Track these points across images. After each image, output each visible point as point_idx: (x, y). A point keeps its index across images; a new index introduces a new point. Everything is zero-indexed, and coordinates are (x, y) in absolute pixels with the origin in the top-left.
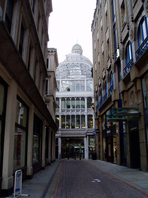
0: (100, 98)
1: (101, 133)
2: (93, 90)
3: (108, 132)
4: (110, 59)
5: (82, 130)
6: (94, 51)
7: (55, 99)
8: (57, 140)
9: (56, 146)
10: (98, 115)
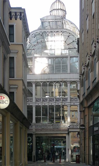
0: (86, 82)
1: (87, 129)
2: (78, 71)
3: (96, 129)
6: (82, 11)
7: (26, 84)
9: (29, 146)
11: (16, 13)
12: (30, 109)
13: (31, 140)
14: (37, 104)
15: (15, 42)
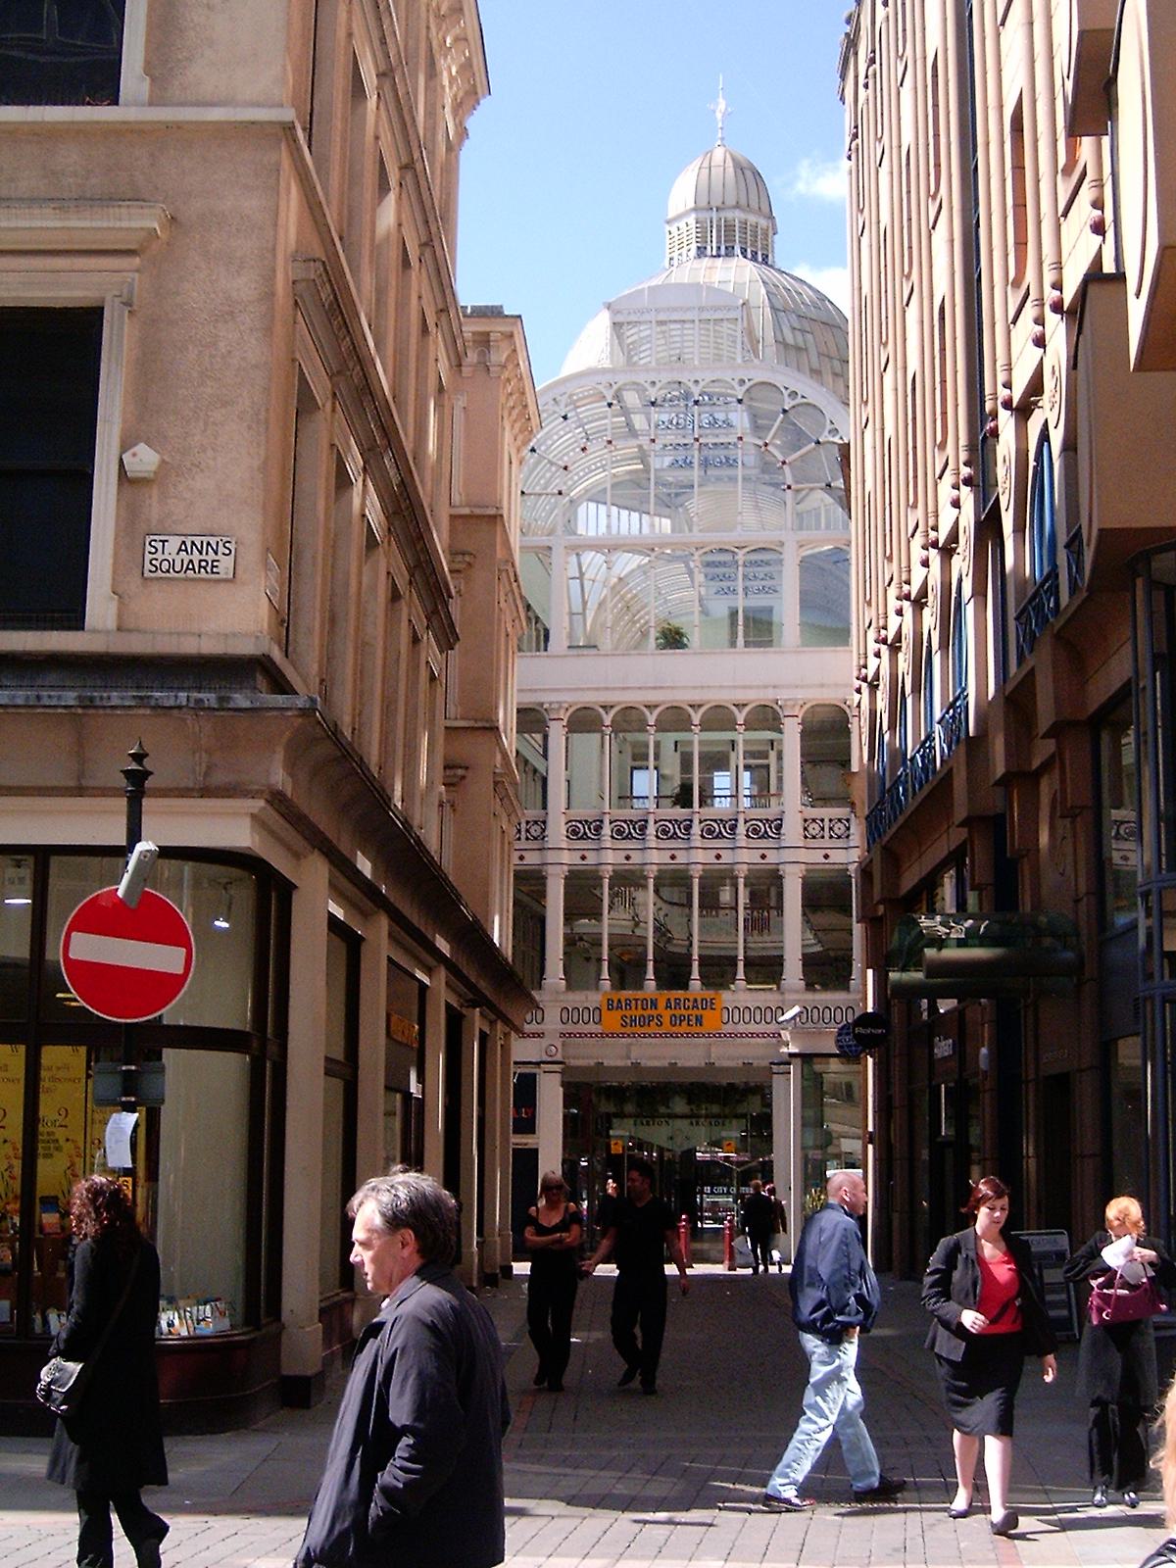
4: (1086, 194)
5: (775, 1023)
8: (526, 1090)
10: (1045, 714)
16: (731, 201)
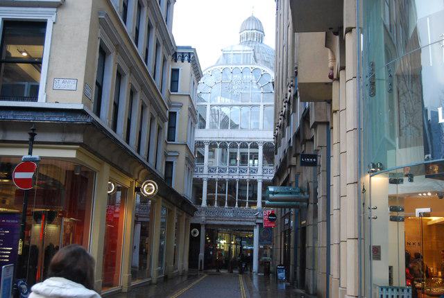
11: (183, 53)
12: (197, 186)
13: (192, 232)
14: (210, 177)
15: (180, 92)
16: (254, 28)
